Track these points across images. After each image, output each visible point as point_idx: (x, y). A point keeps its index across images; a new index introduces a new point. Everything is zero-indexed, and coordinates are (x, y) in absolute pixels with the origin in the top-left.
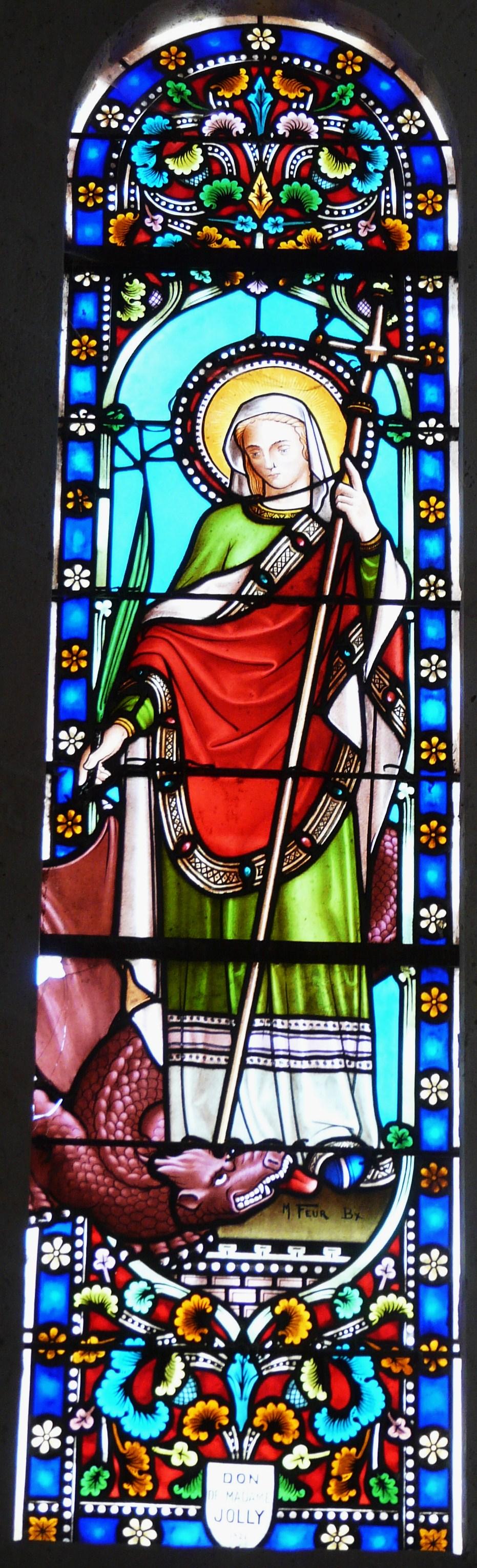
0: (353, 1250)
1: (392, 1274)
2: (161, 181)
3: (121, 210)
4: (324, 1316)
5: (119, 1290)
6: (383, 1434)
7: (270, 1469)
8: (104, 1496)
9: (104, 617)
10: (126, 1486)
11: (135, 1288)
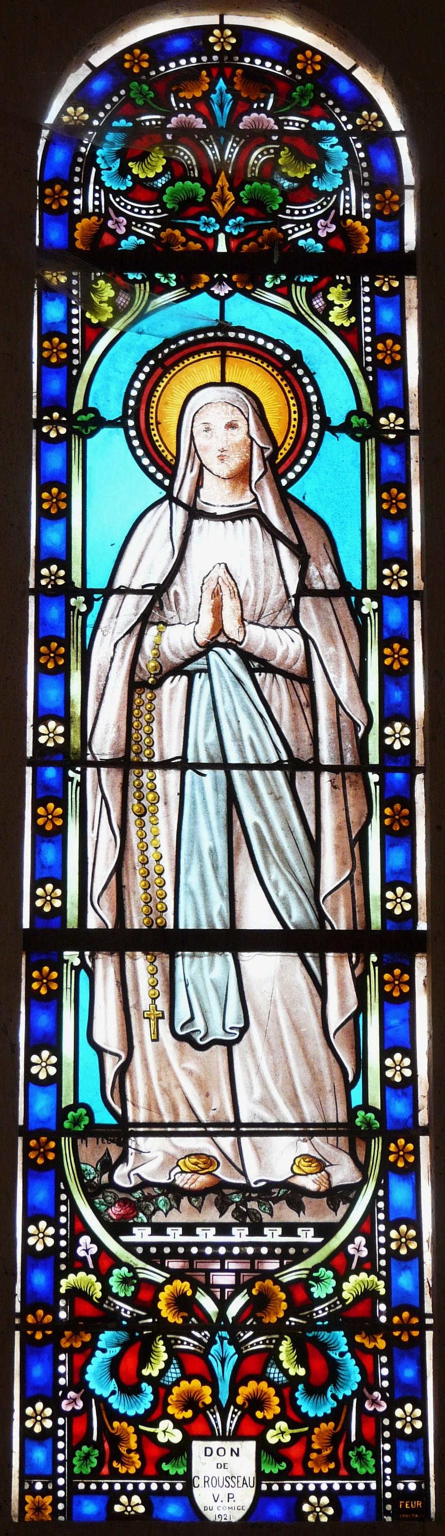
0: (326, 1231)
1: (364, 1253)
3: (85, 213)
4: (300, 1296)
5: (104, 1278)
6: (361, 1407)
8: (96, 1474)
10: (115, 1464)
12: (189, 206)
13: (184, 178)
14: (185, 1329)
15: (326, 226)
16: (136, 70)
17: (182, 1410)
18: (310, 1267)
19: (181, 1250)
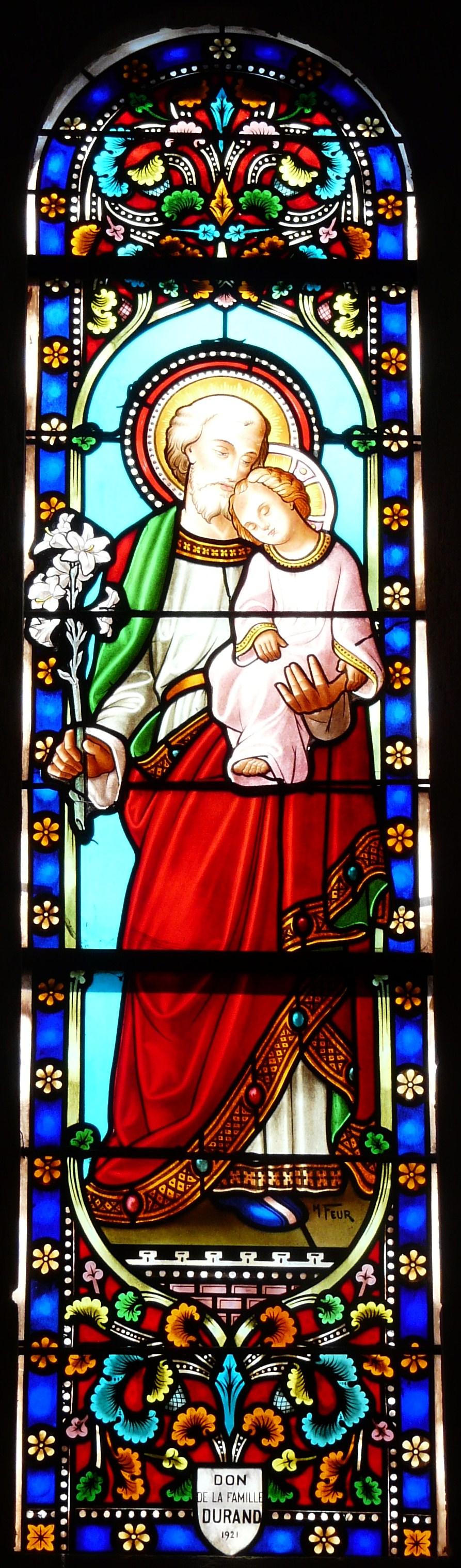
0: (337, 1255)
1: (372, 1281)
5: (109, 1302)
6: (368, 1440)
7: (259, 1472)
8: (100, 1504)
10: (119, 1490)
11: (125, 1299)
12: (188, 216)
13: (182, 186)
14: (188, 1354)
15: (328, 233)
17: (185, 1436)
19: (176, 1274)
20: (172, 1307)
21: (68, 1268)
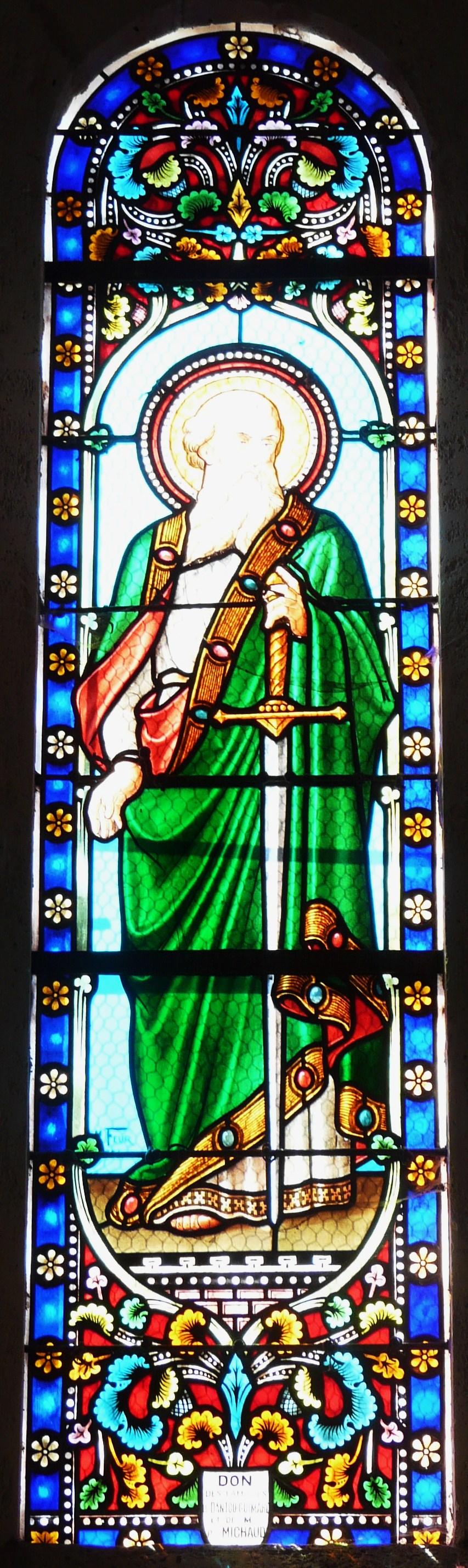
1: (382, 1282)
2: (138, 192)
3: (99, 225)
5: (114, 1310)
6: (378, 1441)
7: (265, 1474)
9: (90, 630)
10: (124, 1499)
11: (129, 1305)
16: (148, 78)
18: (326, 1296)
20: (178, 1313)
21: (72, 1276)
